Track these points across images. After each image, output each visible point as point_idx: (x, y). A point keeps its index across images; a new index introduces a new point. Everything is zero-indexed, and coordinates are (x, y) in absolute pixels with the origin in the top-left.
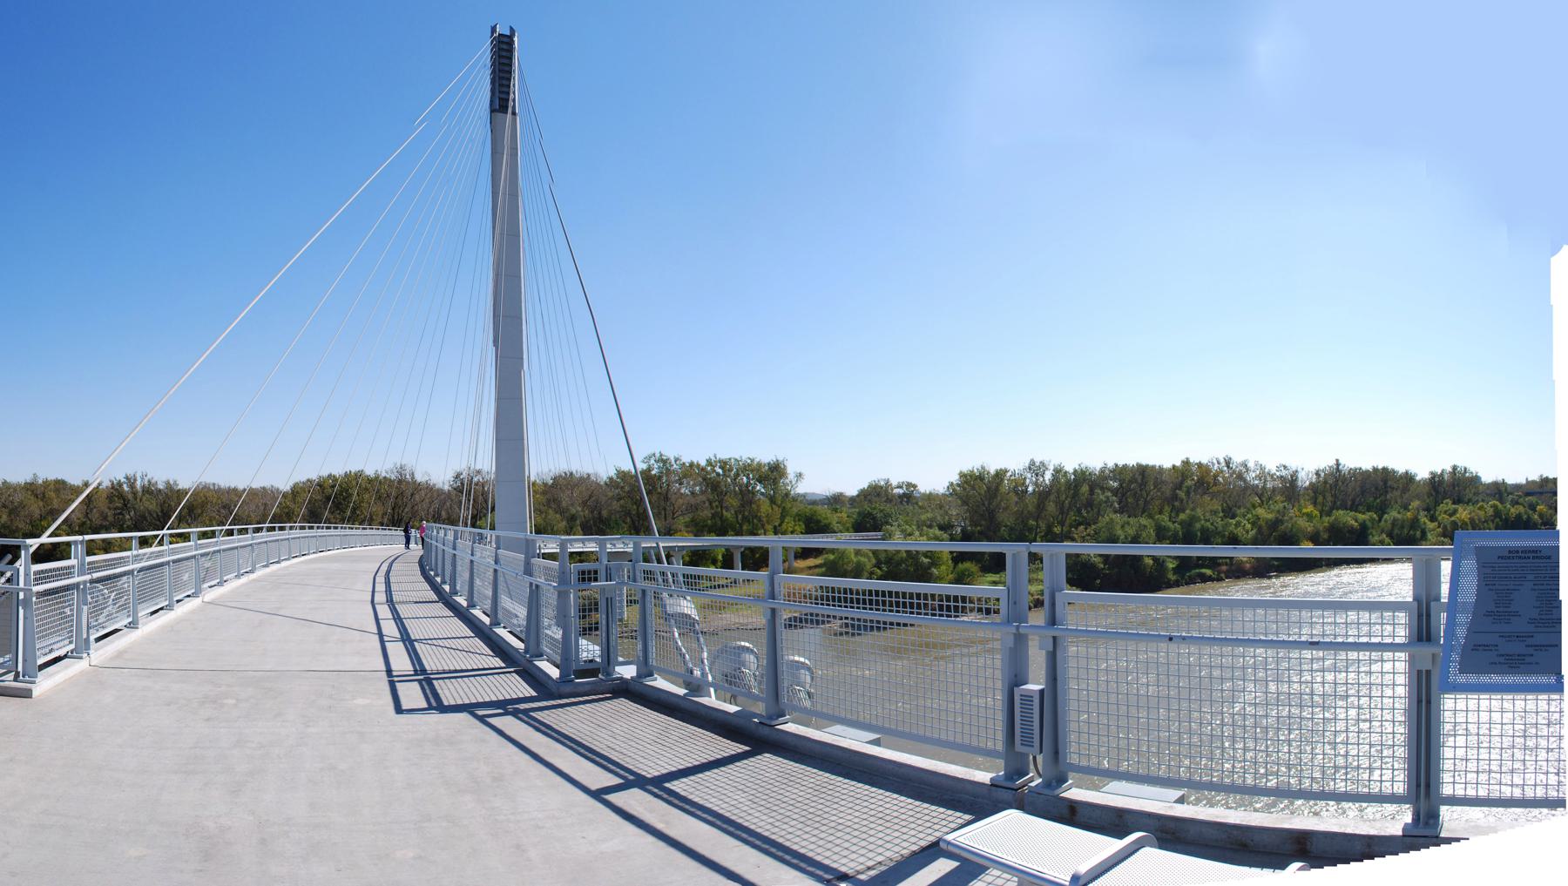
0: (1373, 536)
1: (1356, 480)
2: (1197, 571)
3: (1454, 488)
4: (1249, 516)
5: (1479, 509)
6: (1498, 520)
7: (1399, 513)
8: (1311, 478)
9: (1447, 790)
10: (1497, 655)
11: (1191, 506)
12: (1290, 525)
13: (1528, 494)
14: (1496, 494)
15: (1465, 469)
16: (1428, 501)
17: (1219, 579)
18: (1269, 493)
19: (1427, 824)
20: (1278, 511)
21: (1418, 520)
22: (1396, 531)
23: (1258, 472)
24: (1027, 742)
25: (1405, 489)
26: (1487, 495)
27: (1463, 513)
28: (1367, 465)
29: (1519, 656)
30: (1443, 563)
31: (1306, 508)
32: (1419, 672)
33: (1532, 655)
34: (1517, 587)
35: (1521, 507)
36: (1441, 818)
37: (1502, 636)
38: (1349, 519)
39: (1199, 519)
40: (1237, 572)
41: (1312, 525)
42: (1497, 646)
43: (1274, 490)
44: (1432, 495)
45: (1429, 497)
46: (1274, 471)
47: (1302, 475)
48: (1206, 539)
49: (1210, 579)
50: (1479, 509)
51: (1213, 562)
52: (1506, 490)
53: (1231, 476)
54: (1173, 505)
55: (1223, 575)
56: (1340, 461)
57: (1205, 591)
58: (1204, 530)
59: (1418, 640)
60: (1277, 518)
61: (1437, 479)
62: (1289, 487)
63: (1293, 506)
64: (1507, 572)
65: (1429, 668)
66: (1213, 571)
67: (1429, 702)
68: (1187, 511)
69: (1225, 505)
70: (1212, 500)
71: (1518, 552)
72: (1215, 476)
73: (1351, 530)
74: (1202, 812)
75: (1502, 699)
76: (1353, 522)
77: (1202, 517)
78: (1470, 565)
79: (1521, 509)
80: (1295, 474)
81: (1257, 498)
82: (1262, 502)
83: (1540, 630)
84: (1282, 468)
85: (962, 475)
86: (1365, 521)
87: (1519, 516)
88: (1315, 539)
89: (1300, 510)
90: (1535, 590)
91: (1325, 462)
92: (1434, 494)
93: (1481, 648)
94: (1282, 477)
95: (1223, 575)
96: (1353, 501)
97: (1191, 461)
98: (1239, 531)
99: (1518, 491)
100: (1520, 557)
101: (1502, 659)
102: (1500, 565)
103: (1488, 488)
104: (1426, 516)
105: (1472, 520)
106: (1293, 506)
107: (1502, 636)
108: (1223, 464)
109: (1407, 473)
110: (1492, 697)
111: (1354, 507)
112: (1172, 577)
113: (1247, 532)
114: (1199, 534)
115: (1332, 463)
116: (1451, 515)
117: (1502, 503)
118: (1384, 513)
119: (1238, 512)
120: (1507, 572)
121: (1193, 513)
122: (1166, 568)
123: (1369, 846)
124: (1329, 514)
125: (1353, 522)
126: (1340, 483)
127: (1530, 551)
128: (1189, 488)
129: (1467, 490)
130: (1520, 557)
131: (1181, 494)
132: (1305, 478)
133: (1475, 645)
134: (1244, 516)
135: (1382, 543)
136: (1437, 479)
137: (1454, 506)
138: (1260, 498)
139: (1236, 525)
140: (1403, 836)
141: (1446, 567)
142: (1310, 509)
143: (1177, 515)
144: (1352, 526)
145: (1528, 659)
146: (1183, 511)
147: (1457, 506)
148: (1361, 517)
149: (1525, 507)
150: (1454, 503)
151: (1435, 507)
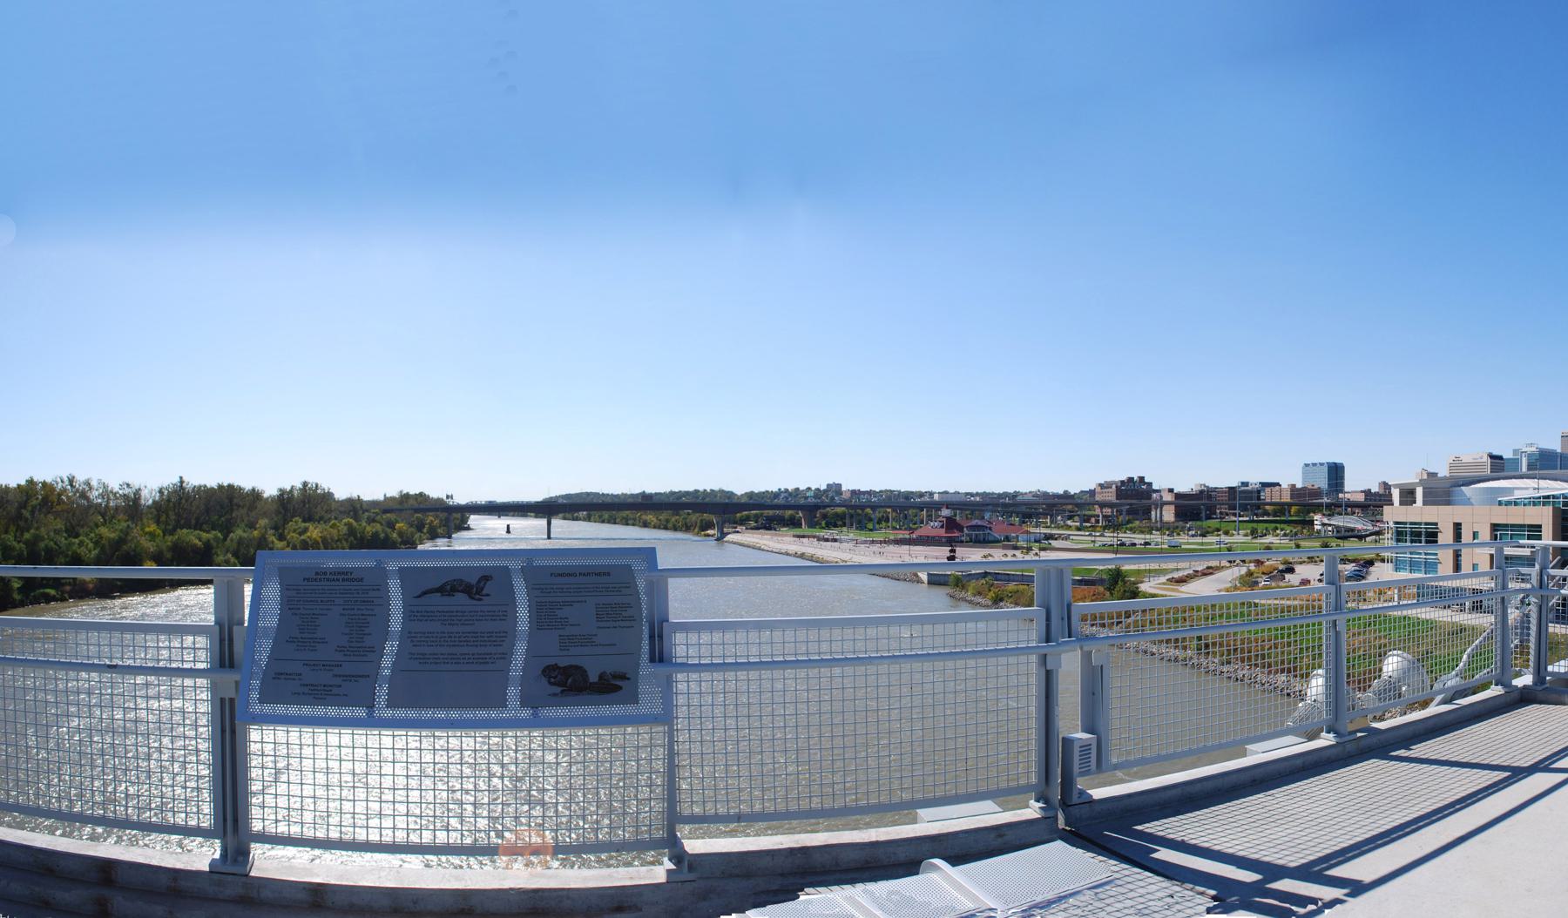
0: (218, 555)
1: (200, 498)
2: (42, 591)
3: (304, 505)
4: (93, 535)
5: (331, 527)
6: (352, 538)
7: (244, 531)
8: (155, 496)
9: (257, 826)
10: (301, 685)
11: (36, 525)
12: (133, 546)
13: (386, 511)
14: (350, 511)
15: (317, 485)
16: (276, 519)
17: (63, 600)
18: (112, 512)
19: (235, 861)
20: (121, 530)
21: (265, 539)
22: (243, 551)
23: (101, 491)
24: (1086, 747)
25: (252, 507)
26: (341, 512)
27: (314, 532)
28: (212, 483)
29: (324, 686)
30: (246, 586)
31: (149, 527)
32: (222, 700)
33: (340, 686)
34: (325, 612)
35: (378, 525)
36: (251, 855)
37: (307, 665)
38: (193, 538)
39: (42, 539)
40: (81, 592)
41: (155, 544)
42: (300, 674)
43: (117, 508)
44: (281, 513)
45: (277, 515)
46: (116, 489)
47: (145, 493)
48: (50, 558)
49: (54, 599)
50: (331, 527)
51: (56, 583)
52: (361, 507)
53: (75, 494)
54: (18, 525)
55: (66, 595)
56: (184, 479)
57: (48, 611)
58: (48, 551)
59: (221, 667)
60: (120, 537)
61: (286, 496)
62: (132, 505)
63: (136, 525)
64: (313, 595)
65: (233, 695)
66: (57, 591)
67: (233, 732)
68: (32, 531)
69: (68, 524)
70: (55, 519)
71: (325, 573)
72: (60, 495)
73: (195, 549)
74: (11, 834)
75: (353, 734)
76: (197, 541)
77: (46, 536)
78: (273, 591)
79: (378, 527)
80: (138, 492)
81: (100, 517)
82: (105, 521)
83: (348, 658)
84: (125, 487)
85: (253, 490)
86: (209, 541)
87: (376, 535)
88: (159, 559)
89: (142, 529)
90: (343, 615)
91: (169, 480)
92: (283, 512)
93: (283, 677)
94: (125, 495)
95: (66, 595)
96: (197, 519)
97: (35, 480)
98: (82, 551)
99: (375, 508)
100: (328, 580)
101: (306, 690)
102: (306, 587)
103: (341, 506)
104: (274, 535)
105: (324, 539)
106: (136, 525)
107: (307, 665)
108: (67, 483)
109: (253, 490)
110: (355, 732)
111: (198, 526)
112: (17, 596)
113: (90, 551)
114: (43, 553)
115: (176, 480)
116: (300, 534)
117: (356, 520)
118: (229, 532)
119: (81, 531)
120: (313, 595)
121: (37, 532)
122: (11, 589)
123: (175, 879)
124: (172, 532)
125: (197, 541)
126: (183, 501)
127: (339, 573)
128: (34, 507)
129: (319, 508)
130: (328, 580)
131: (26, 513)
132: (149, 496)
133: (275, 674)
134: (87, 535)
135: (227, 563)
136: (286, 496)
137: (303, 524)
138: (103, 517)
139: (79, 544)
140: (211, 872)
141: (248, 590)
142: (153, 527)
143: (22, 535)
144: (195, 545)
145: (335, 690)
146: (28, 531)
147: (307, 524)
148: (205, 535)
149: (382, 525)
150: (304, 521)
151: (284, 525)
